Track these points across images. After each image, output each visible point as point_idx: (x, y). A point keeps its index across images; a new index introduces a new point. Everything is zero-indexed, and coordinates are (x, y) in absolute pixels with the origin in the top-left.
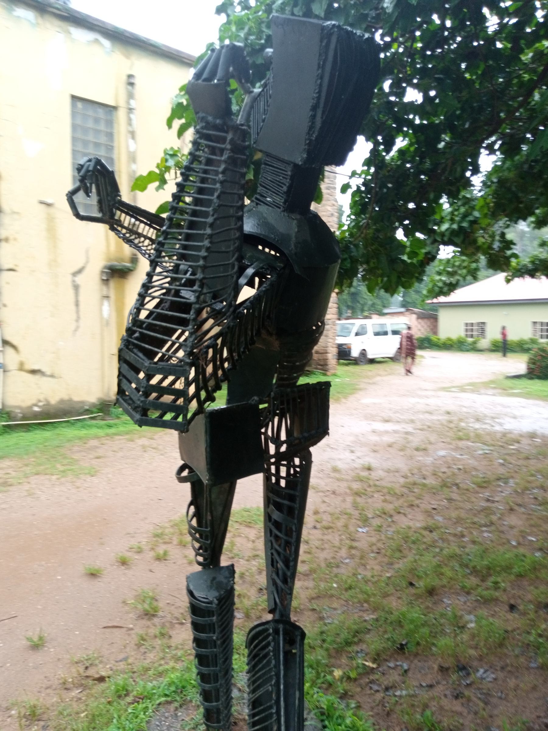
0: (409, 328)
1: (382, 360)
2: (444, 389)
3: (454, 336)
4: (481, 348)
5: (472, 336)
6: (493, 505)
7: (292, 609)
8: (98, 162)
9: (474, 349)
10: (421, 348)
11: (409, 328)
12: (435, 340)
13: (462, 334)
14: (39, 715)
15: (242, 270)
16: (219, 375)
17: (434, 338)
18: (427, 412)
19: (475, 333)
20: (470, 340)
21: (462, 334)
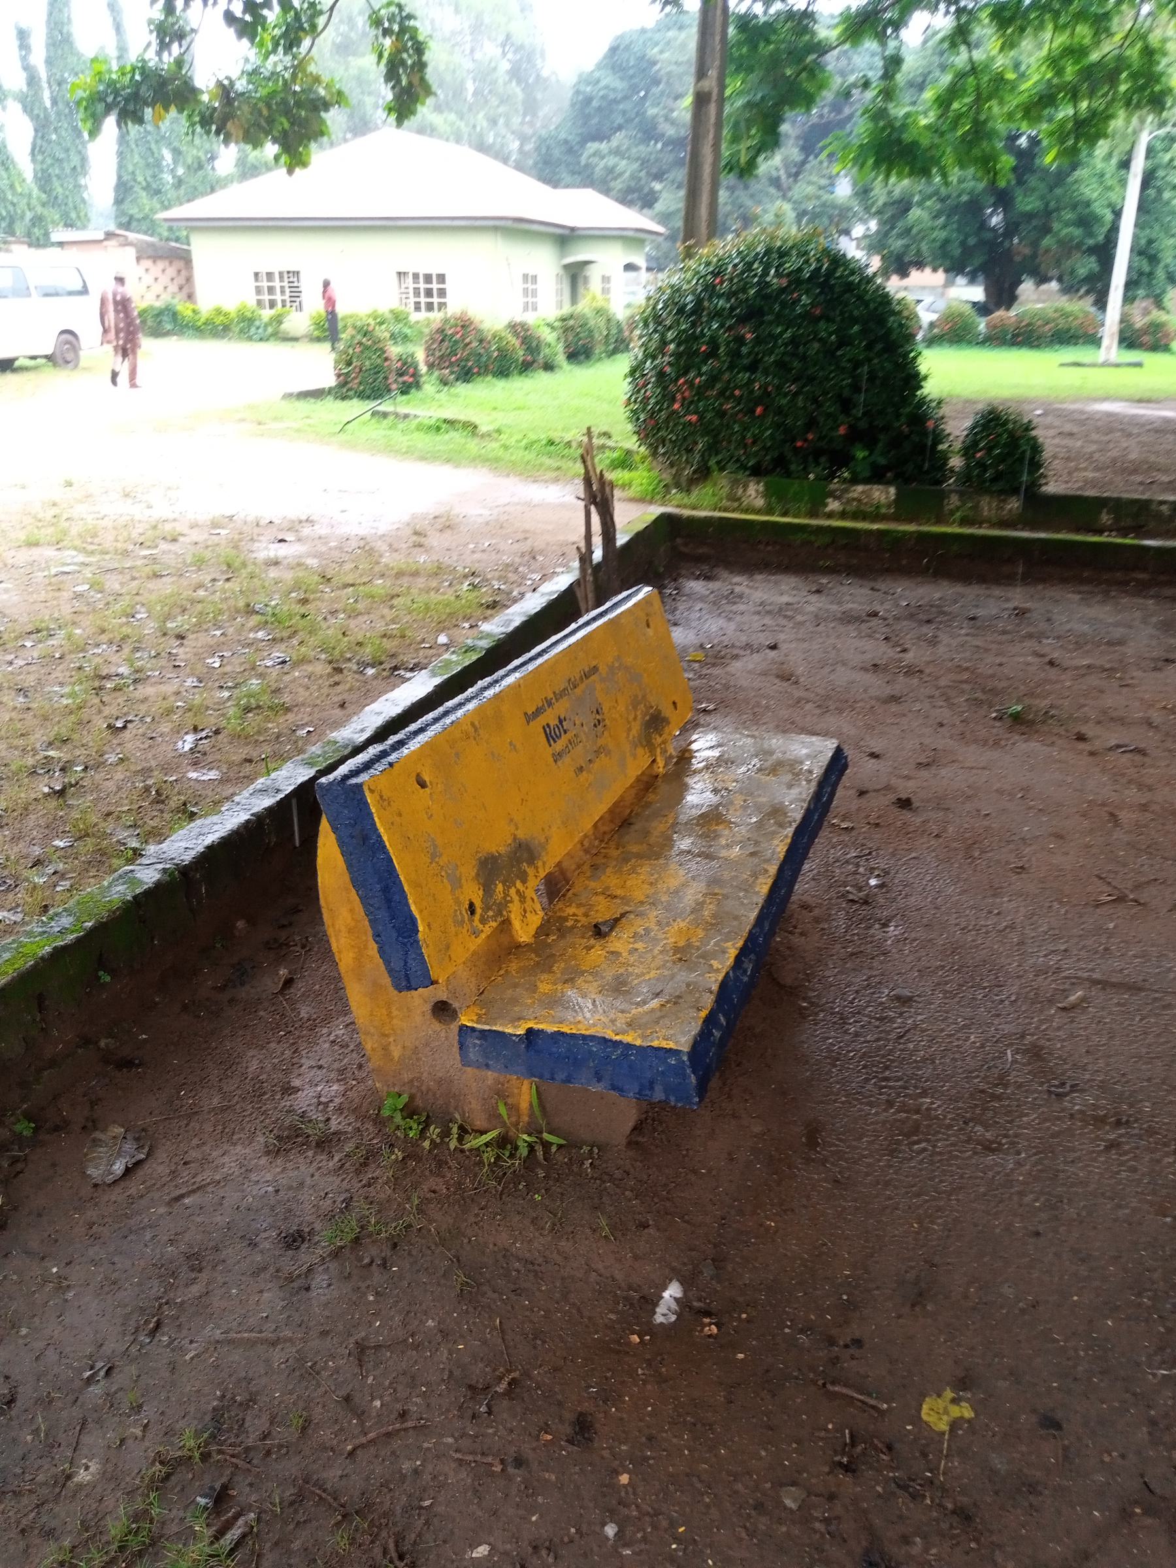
0: (120, 280)
1: (32, 363)
2: (617, 920)
3: (231, 306)
4: (292, 334)
5: (272, 304)
6: (43, 73)
7: (687, 165)
8: (322, 134)
9: (276, 333)
10: (157, 332)
11: (120, 280)
12: (189, 313)
13: (251, 301)
14: (1104, 111)
15: (79, 134)
16: (729, 36)
17: (184, 309)
18: (1140, 401)
19: (278, 297)
20: (266, 314)
21: (251, 301)
